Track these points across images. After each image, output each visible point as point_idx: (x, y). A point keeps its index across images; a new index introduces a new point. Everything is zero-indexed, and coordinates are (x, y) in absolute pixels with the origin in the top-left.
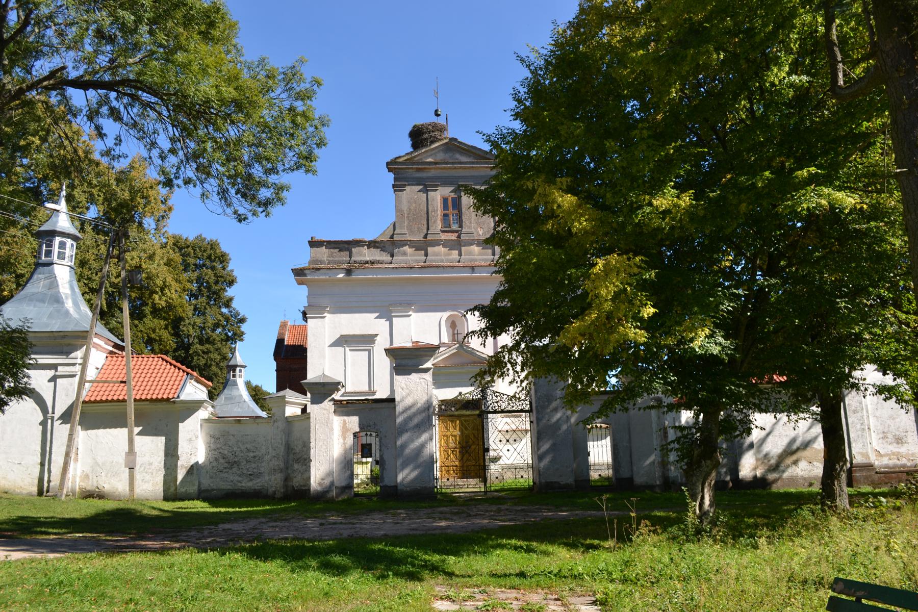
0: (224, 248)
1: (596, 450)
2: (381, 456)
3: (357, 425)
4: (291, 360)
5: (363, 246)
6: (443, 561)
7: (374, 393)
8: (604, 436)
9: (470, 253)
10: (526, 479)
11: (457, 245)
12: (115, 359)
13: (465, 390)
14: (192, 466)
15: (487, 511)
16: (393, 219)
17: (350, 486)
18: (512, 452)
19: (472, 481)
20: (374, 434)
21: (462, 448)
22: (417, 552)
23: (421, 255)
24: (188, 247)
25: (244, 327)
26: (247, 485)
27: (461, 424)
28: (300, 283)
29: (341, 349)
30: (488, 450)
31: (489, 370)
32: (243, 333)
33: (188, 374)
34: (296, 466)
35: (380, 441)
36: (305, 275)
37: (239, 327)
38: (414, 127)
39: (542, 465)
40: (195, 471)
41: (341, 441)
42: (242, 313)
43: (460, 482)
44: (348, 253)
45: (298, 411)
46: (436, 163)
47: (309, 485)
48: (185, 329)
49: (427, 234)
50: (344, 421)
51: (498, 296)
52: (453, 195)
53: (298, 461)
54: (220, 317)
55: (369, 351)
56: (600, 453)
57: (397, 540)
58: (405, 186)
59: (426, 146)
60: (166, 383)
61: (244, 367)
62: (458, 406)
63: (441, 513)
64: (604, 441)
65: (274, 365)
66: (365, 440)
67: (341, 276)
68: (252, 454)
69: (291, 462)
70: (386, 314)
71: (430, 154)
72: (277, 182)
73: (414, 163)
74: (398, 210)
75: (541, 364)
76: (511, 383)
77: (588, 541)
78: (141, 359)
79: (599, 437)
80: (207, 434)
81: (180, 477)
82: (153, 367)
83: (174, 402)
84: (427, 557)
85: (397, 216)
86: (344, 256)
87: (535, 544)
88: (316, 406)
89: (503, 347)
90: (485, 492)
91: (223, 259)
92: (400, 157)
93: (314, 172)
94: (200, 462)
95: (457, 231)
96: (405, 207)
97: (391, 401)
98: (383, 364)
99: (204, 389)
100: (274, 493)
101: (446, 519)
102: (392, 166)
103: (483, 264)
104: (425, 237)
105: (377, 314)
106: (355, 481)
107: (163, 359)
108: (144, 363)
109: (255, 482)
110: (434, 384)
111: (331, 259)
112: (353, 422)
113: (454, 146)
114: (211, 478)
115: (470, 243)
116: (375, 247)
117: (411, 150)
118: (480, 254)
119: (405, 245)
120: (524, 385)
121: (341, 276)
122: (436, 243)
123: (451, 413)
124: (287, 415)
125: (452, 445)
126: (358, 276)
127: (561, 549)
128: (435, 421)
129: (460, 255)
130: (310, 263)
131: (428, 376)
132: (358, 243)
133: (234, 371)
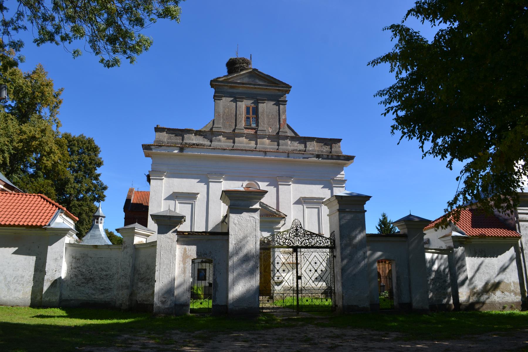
0: (97, 143)
2: (214, 280)
4: (136, 212)
5: (192, 133)
9: (263, 143)
11: (255, 137)
12: (4, 195)
14: (56, 280)
23: (230, 143)
24: (74, 141)
25: (106, 193)
26: (99, 297)
28: (147, 156)
32: (105, 196)
33: (59, 209)
34: (140, 284)
36: (151, 149)
37: (103, 192)
38: (230, 59)
40: (58, 285)
41: (182, 265)
42: (105, 183)
44: (181, 138)
46: (243, 84)
48: (68, 190)
50: (185, 249)
53: (142, 280)
54: (91, 185)
55: (192, 204)
60: (41, 214)
61: (104, 217)
65: (123, 215)
67: (176, 151)
68: (105, 273)
69: (136, 281)
71: (240, 77)
78: (24, 196)
80: (74, 257)
81: (45, 288)
82: (33, 202)
83: (45, 229)
86: (178, 140)
88: (162, 236)
91: (95, 150)
92: (220, 78)
94: (63, 278)
95: (254, 129)
96: (221, 110)
99: (72, 222)
100: (121, 305)
102: (214, 83)
104: (234, 130)
105: (199, 180)
107: (42, 197)
108: (27, 199)
109: (105, 295)
111: (170, 140)
112: (192, 250)
113: (256, 74)
114: (71, 290)
115: (263, 137)
119: (220, 135)
121: (176, 151)
122: (241, 135)
124: (135, 243)
126: (188, 152)
129: (256, 144)
132: (189, 131)
133: (98, 219)
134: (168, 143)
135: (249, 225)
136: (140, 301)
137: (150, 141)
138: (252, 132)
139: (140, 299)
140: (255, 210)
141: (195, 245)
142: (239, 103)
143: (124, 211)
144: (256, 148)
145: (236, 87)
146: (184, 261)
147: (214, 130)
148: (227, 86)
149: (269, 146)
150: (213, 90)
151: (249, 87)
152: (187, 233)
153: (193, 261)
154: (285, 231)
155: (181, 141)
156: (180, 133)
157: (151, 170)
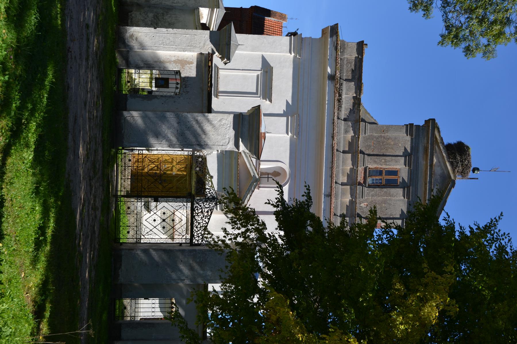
1: (150, 306)
2: (156, 97)
3: (187, 75)
5: (356, 93)
6: (27, 146)
7: (217, 96)
8: (164, 310)
9: (343, 194)
10: (127, 236)
11: (352, 182)
13: (215, 181)
15: (95, 197)
16: (380, 123)
17: (129, 66)
18: (154, 223)
19: (128, 184)
20: (178, 91)
21: (160, 176)
22: (39, 116)
23: (344, 147)
27: (183, 176)
28: (324, 31)
29: (259, 66)
30: (156, 201)
31: (240, 209)
34: (151, 15)
35: (170, 97)
36: (331, 36)
38: (468, 148)
39: (139, 252)
41: (173, 59)
43: (128, 173)
44: (350, 78)
45: (204, 21)
46: (431, 165)
47: (132, 25)
49: (364, 154)
50: (192, 63)
51: (316, 221)
52: (400, 180)
53: (156, 17)
55: (256, 93)
56: (148, 308)
57: (60, 95)
58: (411, 135)
59: (449, 158)
62: (200, 174)
63: (96, 151)
64: (159, 310)
66: (172, 84)
67: (329, 70)
70: (290, 112)
71: (440, 161)
72: (434, 5)
73: (432, 145)
74: (388, 128)
75: (237, 262)
76: (225, 230)
77: (48, 306)
79: (163, 306)
84: (33, 126)
85: (382, 126)
86: (347, 74)
87: (48, 248)
89: (264, 224)
90: (116, 196)
92: (439, 132)
93: (442, 43)
95: (365, 182)
97: (210, 110)
98: (244, 105)
101: (87, 156)
102: (431, 124)
103: (333, 205)
104: (362, 152)
105: (290, 103)
106: (133, 71)
110: (222, 152)
111: (345, 62)
112: (190, 72)
113: (447, 184)
115: (353, 194)
116: (354, 104)
117: (445, 143)
118: (342, 203)
119: (354, 133)
120: (220, 242)
121: (329, 70)
122: (355, 162)
123: (194, 167)
124: (201, 9)
125: (163, 167)
126: (328, 86)
127: (39, 277)
128: (186, 152)
129: (343, 184)
130: (343, 41)
131: (231, 147)
132: (359, 88)
134: (341, 59)
135: (219, 137)
136: (131, 15)
137: (344, 35)
138: (360, 178)
139: (133, 15)
140: (237, 145)
141: (197, 75)
142: (402, 160)
143: (252, 7)
144: (336, 183)
145: (427, 155)
146: (179, 61)
147: (362, 124)
148: (428, 142)
149: (339, 203)
150: (422, 123)
151: (426, 174)
152: (210, 64)
153: (178, 73)
154: (212, 183)
155: (344, 78)
156: (357, 77)
157: (303, 36)
